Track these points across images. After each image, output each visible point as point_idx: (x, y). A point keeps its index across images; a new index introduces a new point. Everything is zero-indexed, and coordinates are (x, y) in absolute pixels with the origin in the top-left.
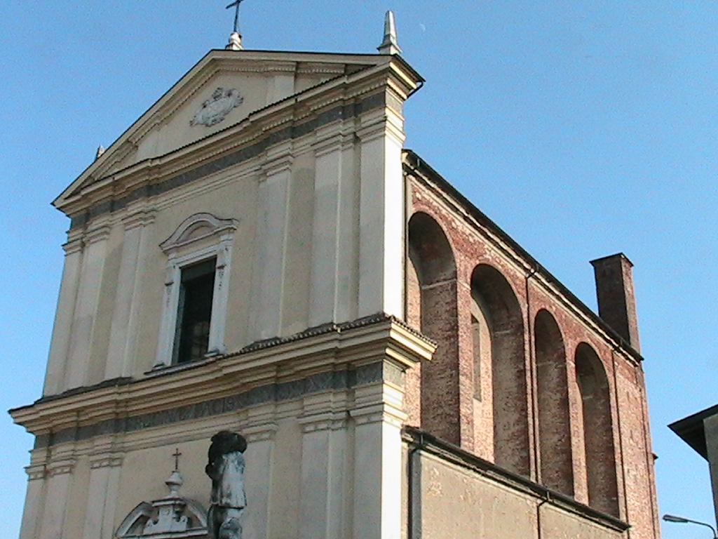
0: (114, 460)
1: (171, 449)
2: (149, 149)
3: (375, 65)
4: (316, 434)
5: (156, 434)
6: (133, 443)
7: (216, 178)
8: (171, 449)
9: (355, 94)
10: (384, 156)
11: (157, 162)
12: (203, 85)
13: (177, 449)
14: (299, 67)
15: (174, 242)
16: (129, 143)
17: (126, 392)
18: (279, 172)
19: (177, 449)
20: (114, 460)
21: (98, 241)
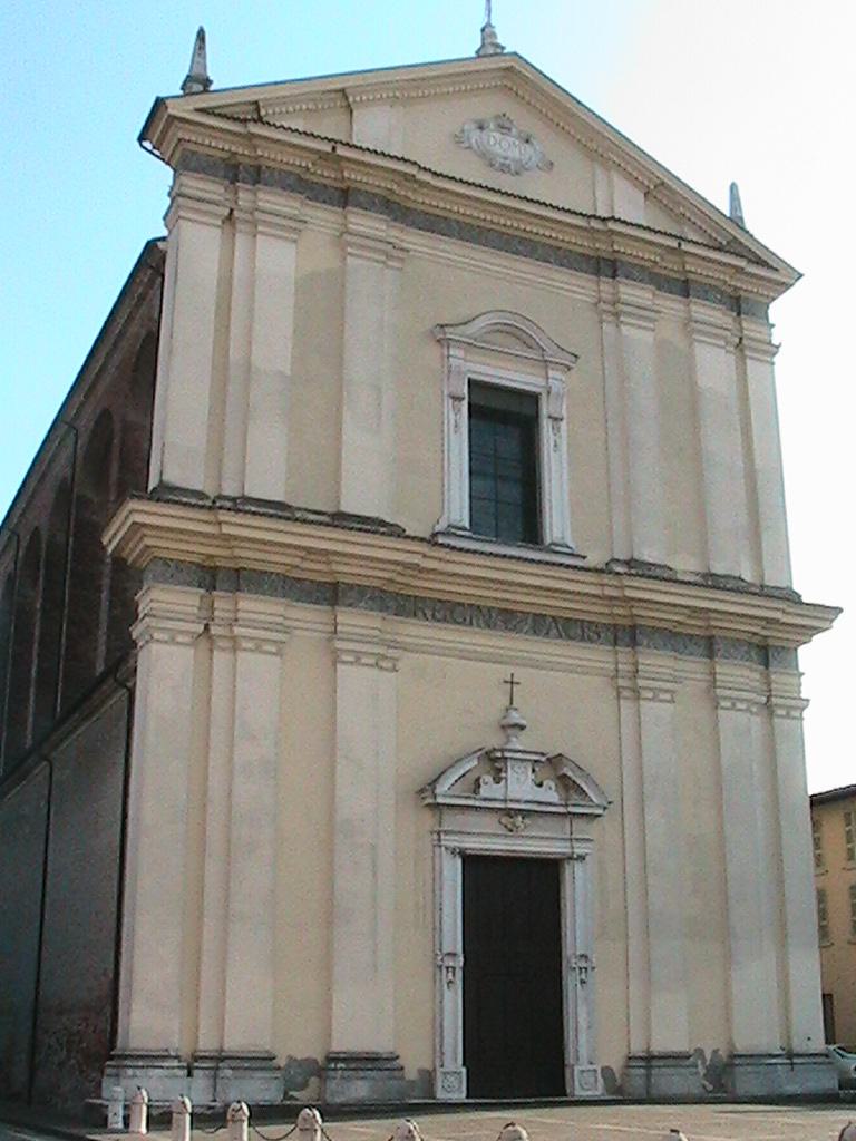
0: (384, 657)
1: (505, 671)
2: (374, 129)
3: (776, 270)
4: (354, 668)
5: (509, 644)
6: (408, 640)
7: (557, 276)
8: (505, 671)
9: (739, 285)
10: (774, 383)
11: (426, 177)
12: (695, 223)
13: (512, 675)
14: (661, 188)
15: (468, 333)
16: (343, 95)
17: (435, 558)
18: (640, 327)
19: (512, 675)
20: (384, 657)
21: (286, 239)
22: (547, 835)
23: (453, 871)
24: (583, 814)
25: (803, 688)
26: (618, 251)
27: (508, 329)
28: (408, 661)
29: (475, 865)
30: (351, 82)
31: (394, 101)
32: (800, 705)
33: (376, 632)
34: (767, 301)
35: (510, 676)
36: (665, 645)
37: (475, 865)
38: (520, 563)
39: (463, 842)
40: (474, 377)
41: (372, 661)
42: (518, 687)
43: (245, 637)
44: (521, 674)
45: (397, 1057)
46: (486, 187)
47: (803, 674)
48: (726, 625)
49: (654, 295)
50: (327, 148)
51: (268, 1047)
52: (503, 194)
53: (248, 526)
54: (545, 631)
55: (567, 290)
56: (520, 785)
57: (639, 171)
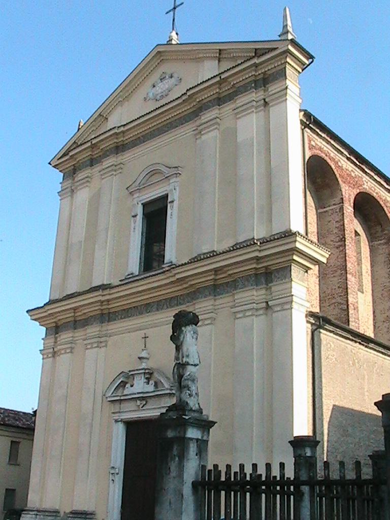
1: (141, 333)
2: (116, 119)
8: (141, 333)
9: (263, 71)
11: (122, 129)
13: (145, 334)
16: (101, 117)
19: (145, 334)
22: (153, 407)
23: (120, 432)
24: (160, 395)
25: (293, 289)
26: (200, 101)
27: (152, 173)
28: (111, 341)
29: (131, 426)
30: (99, 111)
31: (120, 103)
32: (289, 300)
33: (211, 307)
34: (283, 67)
35: (144, 335)
36: (210, 294)
37: (131, 426)
38: (154, 277)
39: (122, 416)
40: (143, 202)
41: (96, 345)
42: (148, 339)
43: (274, 305)
44: (149, 332)
45: (94, 514)
46: (138, 118)
47: (43, 339)
48: (235, 271)
49: (219, 109)
50: (218, 79)
51: (57, 508)
52: (244, 62)
53: (233, 257)
54: (107, 318)
55: (181, 136)
56: (140, 386)
57: (107, 110)
